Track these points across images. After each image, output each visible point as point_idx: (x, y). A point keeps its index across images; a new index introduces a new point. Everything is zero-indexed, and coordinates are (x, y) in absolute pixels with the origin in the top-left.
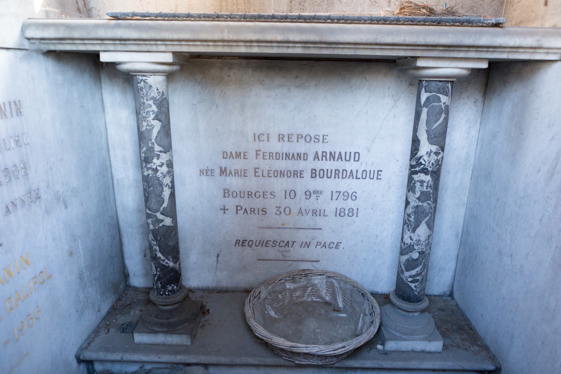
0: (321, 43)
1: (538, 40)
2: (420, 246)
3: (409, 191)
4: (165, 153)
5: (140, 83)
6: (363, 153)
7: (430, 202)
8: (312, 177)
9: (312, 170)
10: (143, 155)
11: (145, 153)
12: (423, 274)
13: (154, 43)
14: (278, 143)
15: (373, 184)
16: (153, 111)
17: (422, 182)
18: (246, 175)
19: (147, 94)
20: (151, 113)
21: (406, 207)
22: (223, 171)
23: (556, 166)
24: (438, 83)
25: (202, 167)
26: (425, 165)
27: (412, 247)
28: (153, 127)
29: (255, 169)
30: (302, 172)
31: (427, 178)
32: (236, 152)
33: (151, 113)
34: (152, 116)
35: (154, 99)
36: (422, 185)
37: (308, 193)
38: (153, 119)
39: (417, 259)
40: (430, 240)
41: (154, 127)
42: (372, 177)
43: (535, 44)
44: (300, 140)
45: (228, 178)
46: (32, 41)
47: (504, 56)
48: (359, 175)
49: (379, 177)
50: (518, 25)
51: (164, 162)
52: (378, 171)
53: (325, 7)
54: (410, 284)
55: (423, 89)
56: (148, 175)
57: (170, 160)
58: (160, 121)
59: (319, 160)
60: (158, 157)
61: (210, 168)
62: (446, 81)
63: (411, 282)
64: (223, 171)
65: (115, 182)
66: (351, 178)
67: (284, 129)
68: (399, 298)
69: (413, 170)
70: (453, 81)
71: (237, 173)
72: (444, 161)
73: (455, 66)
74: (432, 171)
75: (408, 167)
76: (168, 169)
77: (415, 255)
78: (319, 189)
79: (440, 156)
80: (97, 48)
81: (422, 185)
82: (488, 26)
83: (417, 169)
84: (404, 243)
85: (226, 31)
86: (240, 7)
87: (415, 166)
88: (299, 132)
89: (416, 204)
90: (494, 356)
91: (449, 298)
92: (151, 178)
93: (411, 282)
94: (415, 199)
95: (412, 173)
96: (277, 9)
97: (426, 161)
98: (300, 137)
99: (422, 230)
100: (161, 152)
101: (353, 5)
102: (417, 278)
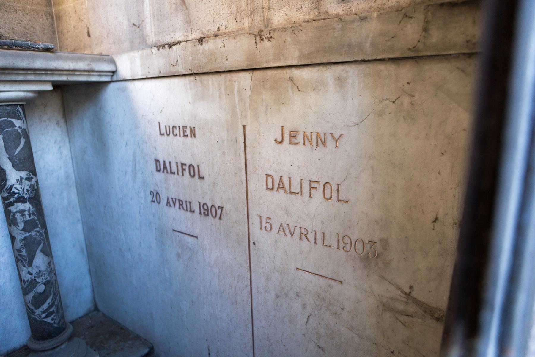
1: (89, 65)
2: (43, 277)
3: (10, 226)
7: (38, 229)
12: (56, 302)
17: (22, 212)
21: (13, 243)
23: (136, 166)
26: (19, 193)
27: (34, 282)
31: (27, 206)
36: (23, 215)
39: (44, 291)
40: (52, 267)
43: (87, 68)
47: (64, 78)
50: (74, 51)
54: (45, 320)
62: (14, 105)
63: (46, 317)
68: (39, 340)
69: (6, 202)
70: (22, 105)
72: (39, 184)
73: (17, 89)
74: (30, 198)
77: (41, 288)
79: (33, 181)
81: (23, 215)
82: (39, 50)
83: (12, 200)
84: (24, 281)
89: (23, 236)
90: (145, 340)
91: (95, 313)
93: (46, 317)
94: (21, 232)
95: (7, 206)
97: (20, 189)
99: (40, 260)
102: (51, 310)
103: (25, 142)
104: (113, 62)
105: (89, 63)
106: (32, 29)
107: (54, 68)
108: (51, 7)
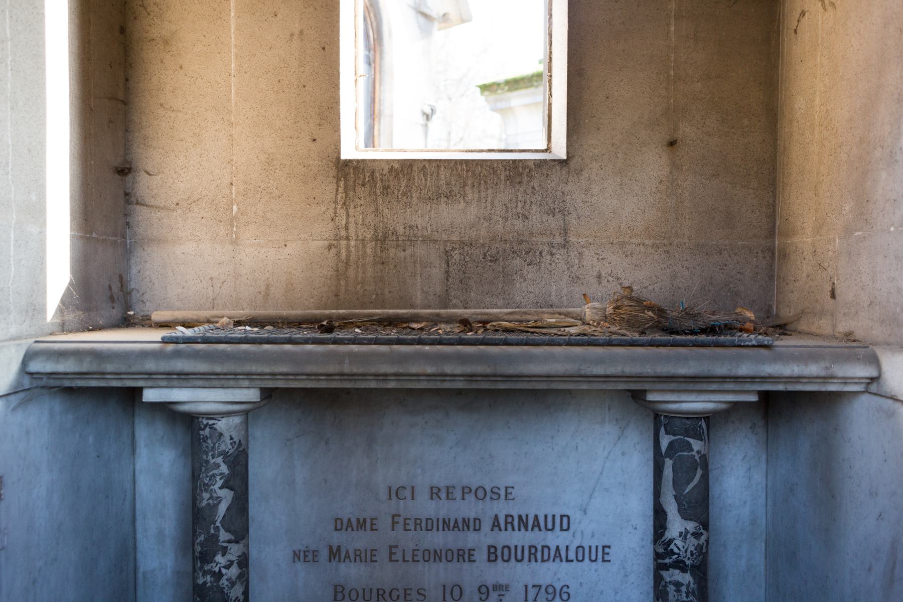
0: (495, 376)
1: (827, 368)
4: (237, 542)
5: (203, 430)
6: (576, 516)
8: (489, 560)
9: (489, 547)
10: (198, 548)
11: (202, 544)
13: (232, 377)
14: (430, 501)
15: (596, 570)
16: (221, 474)
17: (678, 585)
18: (374, 558)
19: (213, 447)
20: (218, 478)
22: (334, 553)
24: (684, 421)
25: (297, 547)
26: (679, 554)
28: (219, 500)
29: (391, 547)
30: (472, 552)
31: (686, 578)
32: (358, 520)
33: (218, 478)
34: (220, 483)
35: (224, 454)
36: (678, 591)
37: (484, 590)
38: (221, 488)
41: (220, 501)
42: (593, 558)
43: (823, 373)
44: (466, 496)
45: (342, 566)
46: (35, 376)
47: (781, 387)
48: (572, 556)
49: (606, 557)
51: (234, 558)
52: (604, 547)
53: (500, 286)
55: (662, 429)
56: (205, 583)
57: (244, 554)
58: (231, 489)
59: (500, 530)
60: (225, 551)
61: (313, 547)
62: (697, 418)
64: (334, 553)
65: (140, 576)
66: (558, 560)
67: (440, 478)
69: (660, 561)
71: (357, 556)
74: (692, 566)
75: (652, 555)
76: (239, 571)
78: (503, 581)
79: (703, 538)
80: (140, 384)
81: (678, 591)
83: (667, 561)
85: (347, 361)
86: (367, 288)
87: (663, 557)
88: (465, 482)
92: (210, 588)
95: (659, 568)
96: (425, 290)
97: (681, 548)
98: (466, 490)
100: (229, 542)
101: (544, 282)
103: (702, 476)
104: (875, 361)
105: (827, 364)
106: (739, 276)
107: (767, 375)
108: (774, 238)
